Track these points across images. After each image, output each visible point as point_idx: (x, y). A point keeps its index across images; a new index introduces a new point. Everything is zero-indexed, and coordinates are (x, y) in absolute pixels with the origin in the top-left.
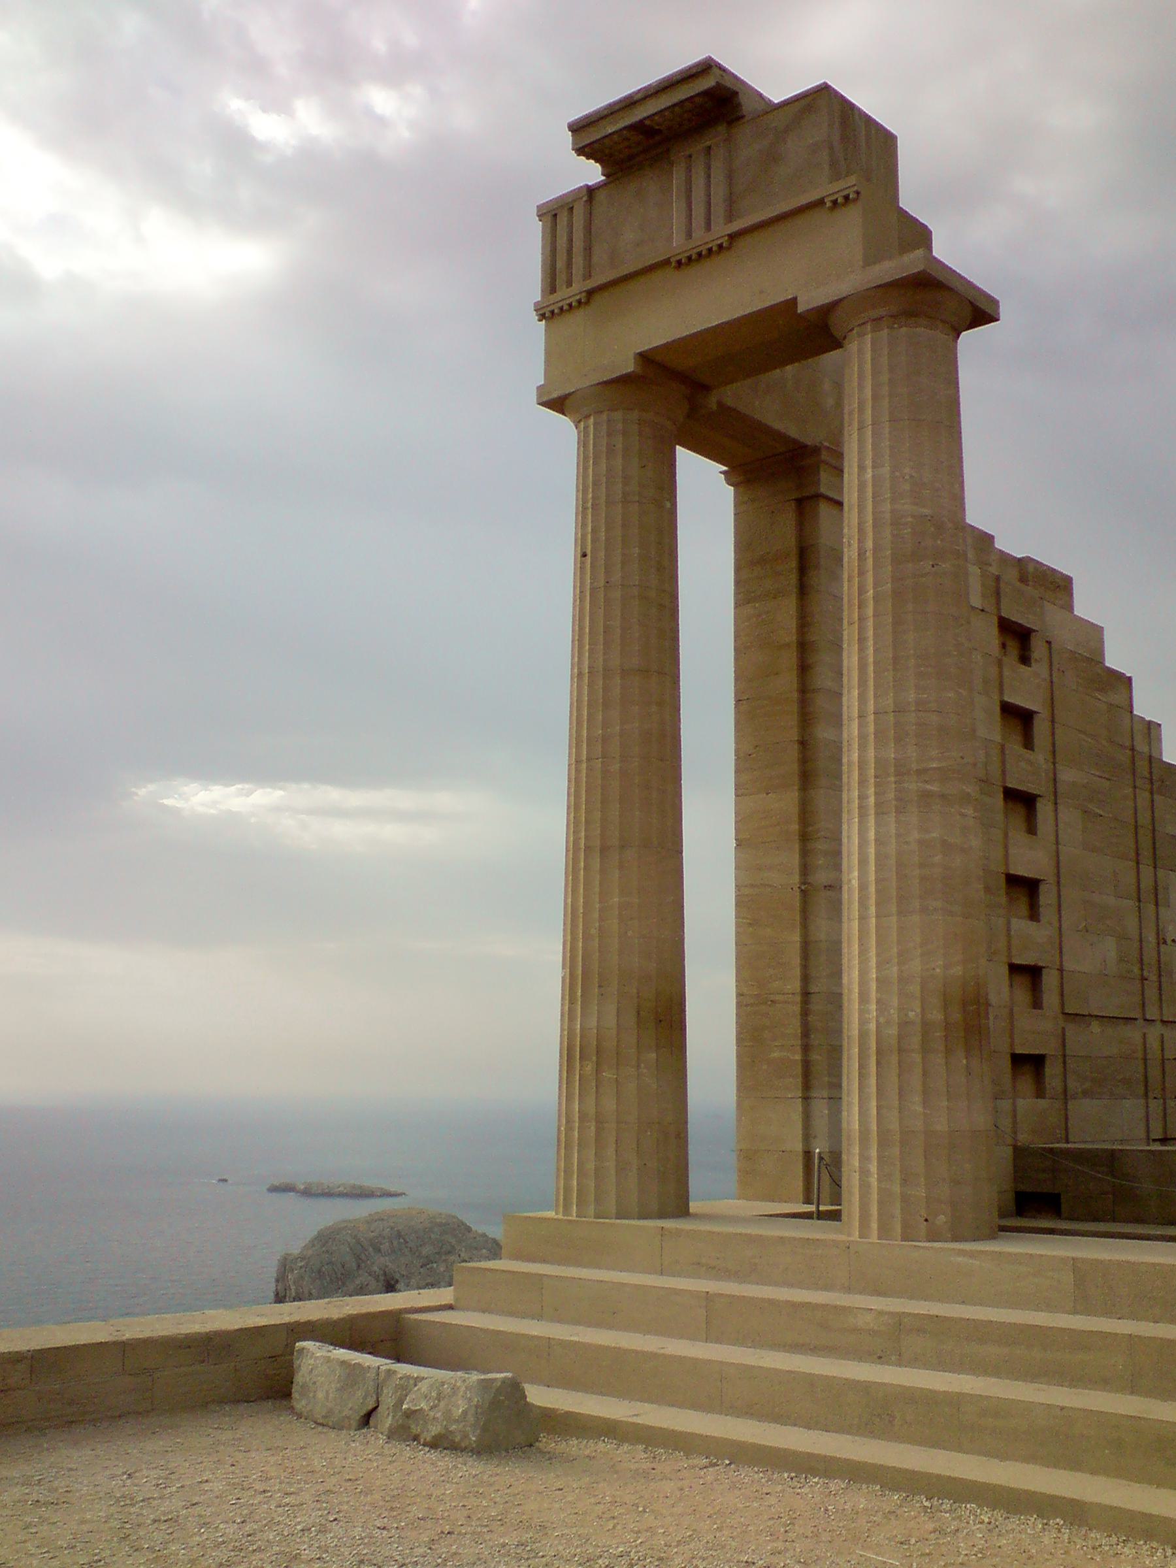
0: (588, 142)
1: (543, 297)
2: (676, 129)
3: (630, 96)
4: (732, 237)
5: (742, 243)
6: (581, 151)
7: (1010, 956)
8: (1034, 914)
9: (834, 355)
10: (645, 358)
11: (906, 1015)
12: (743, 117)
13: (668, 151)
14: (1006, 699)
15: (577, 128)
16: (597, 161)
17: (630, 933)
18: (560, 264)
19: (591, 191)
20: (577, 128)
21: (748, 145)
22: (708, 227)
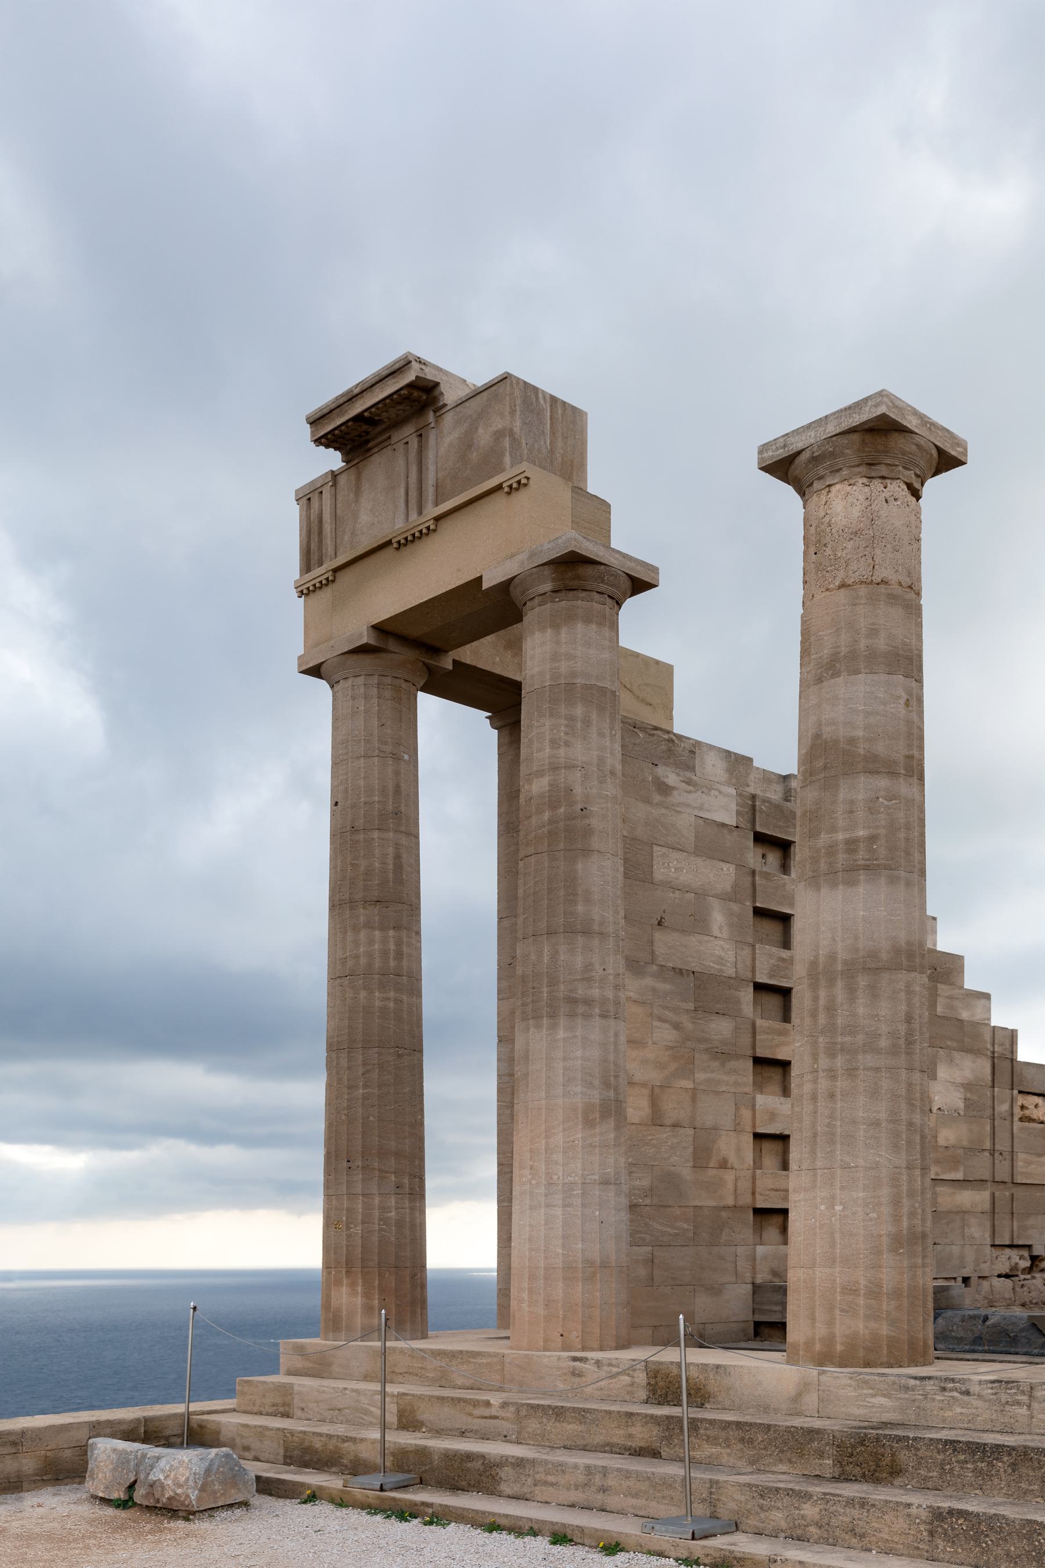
0: (322, 433)
1: (301, 575)
2: (380, 422)
3: (350, 391)
4: (437, 519)
5: (446, 525)
6: (318, 442)
7: (754, 1126)
8: (786, 1092)
9: (519, 625)
10: (379, 628)
11: (551, 1178)
12: (445, 405)
13: (390, 437)
14: (758, 905)
15: (315, 421)
16: (336, 449)
17: (371, 1118)
18: (314, 546)
19: (334, 475)
20: (315, 421)
21: (445, 437)
22: (420, 513)
